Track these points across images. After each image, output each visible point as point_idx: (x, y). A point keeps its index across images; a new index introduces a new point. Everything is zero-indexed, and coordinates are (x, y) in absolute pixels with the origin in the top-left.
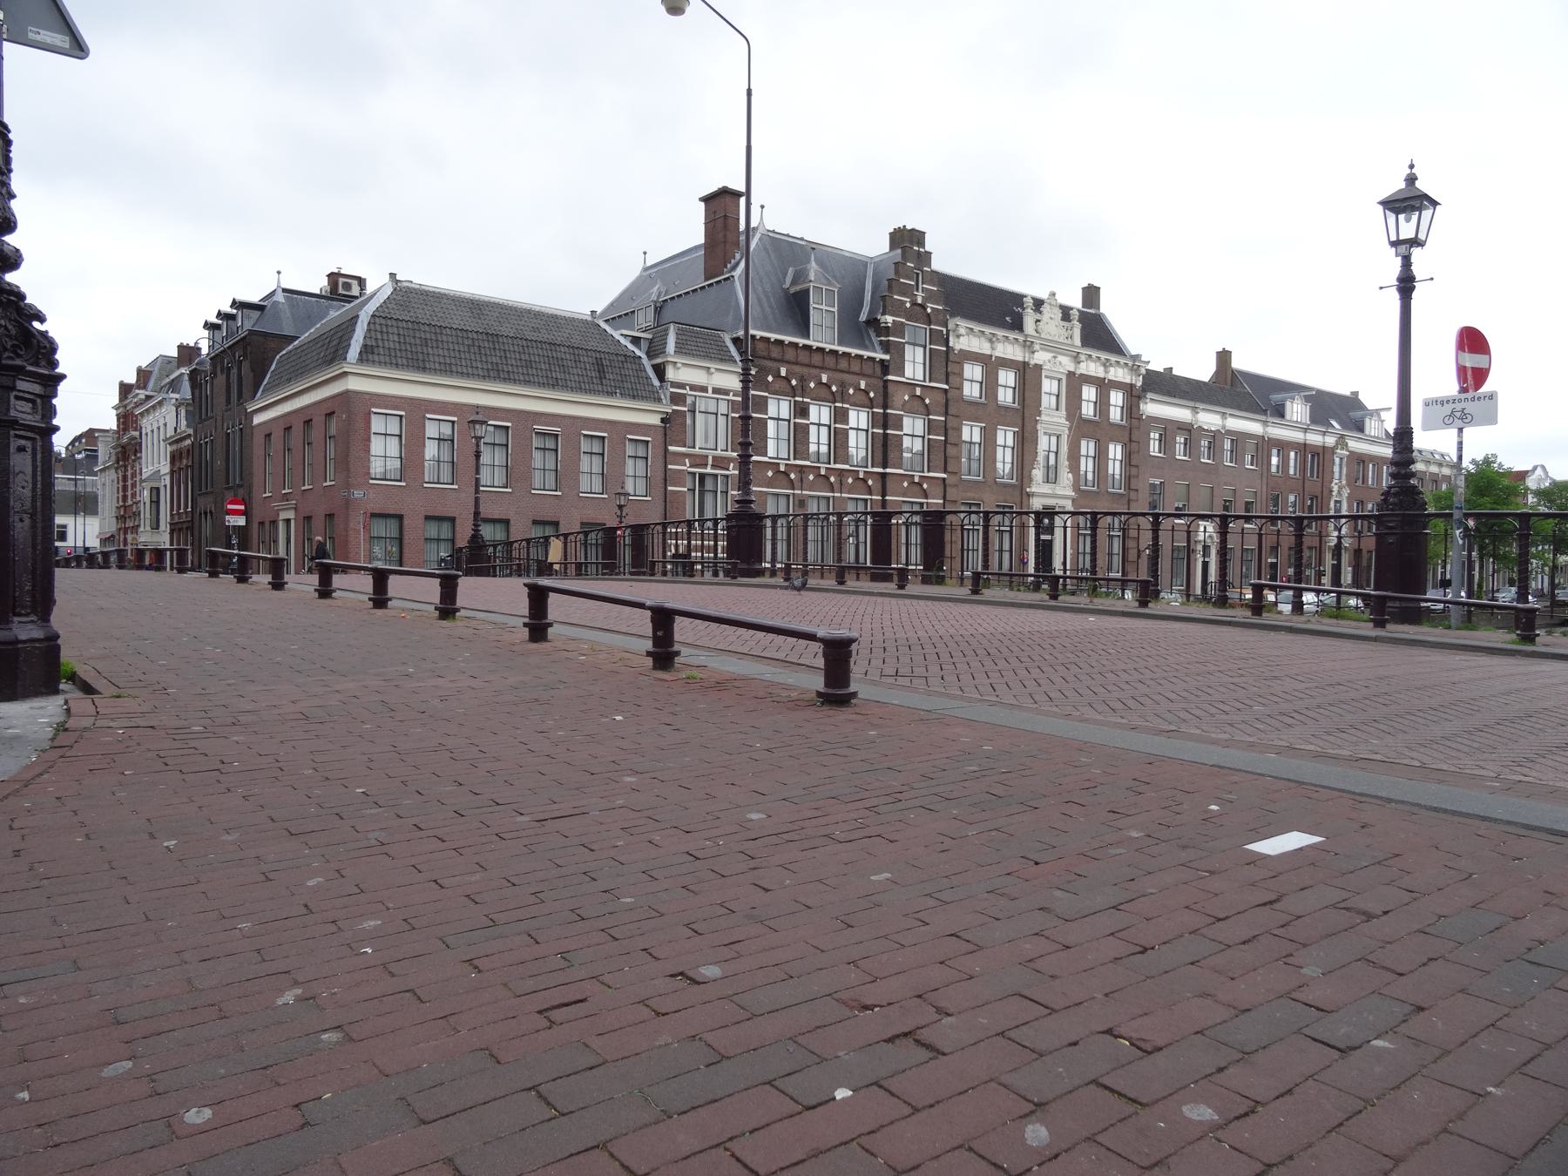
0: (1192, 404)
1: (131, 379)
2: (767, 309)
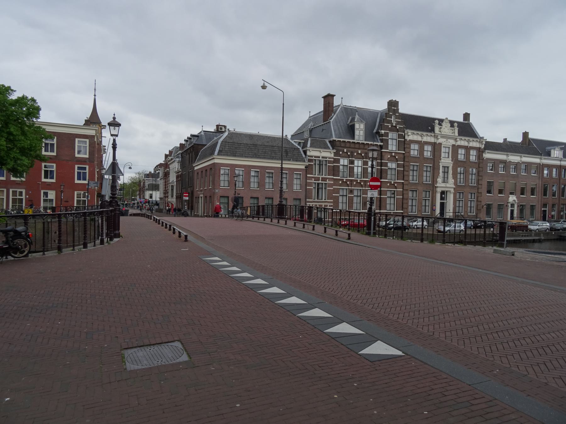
0: (506, 153)
1: (168, 153)
2: (341, 131)
